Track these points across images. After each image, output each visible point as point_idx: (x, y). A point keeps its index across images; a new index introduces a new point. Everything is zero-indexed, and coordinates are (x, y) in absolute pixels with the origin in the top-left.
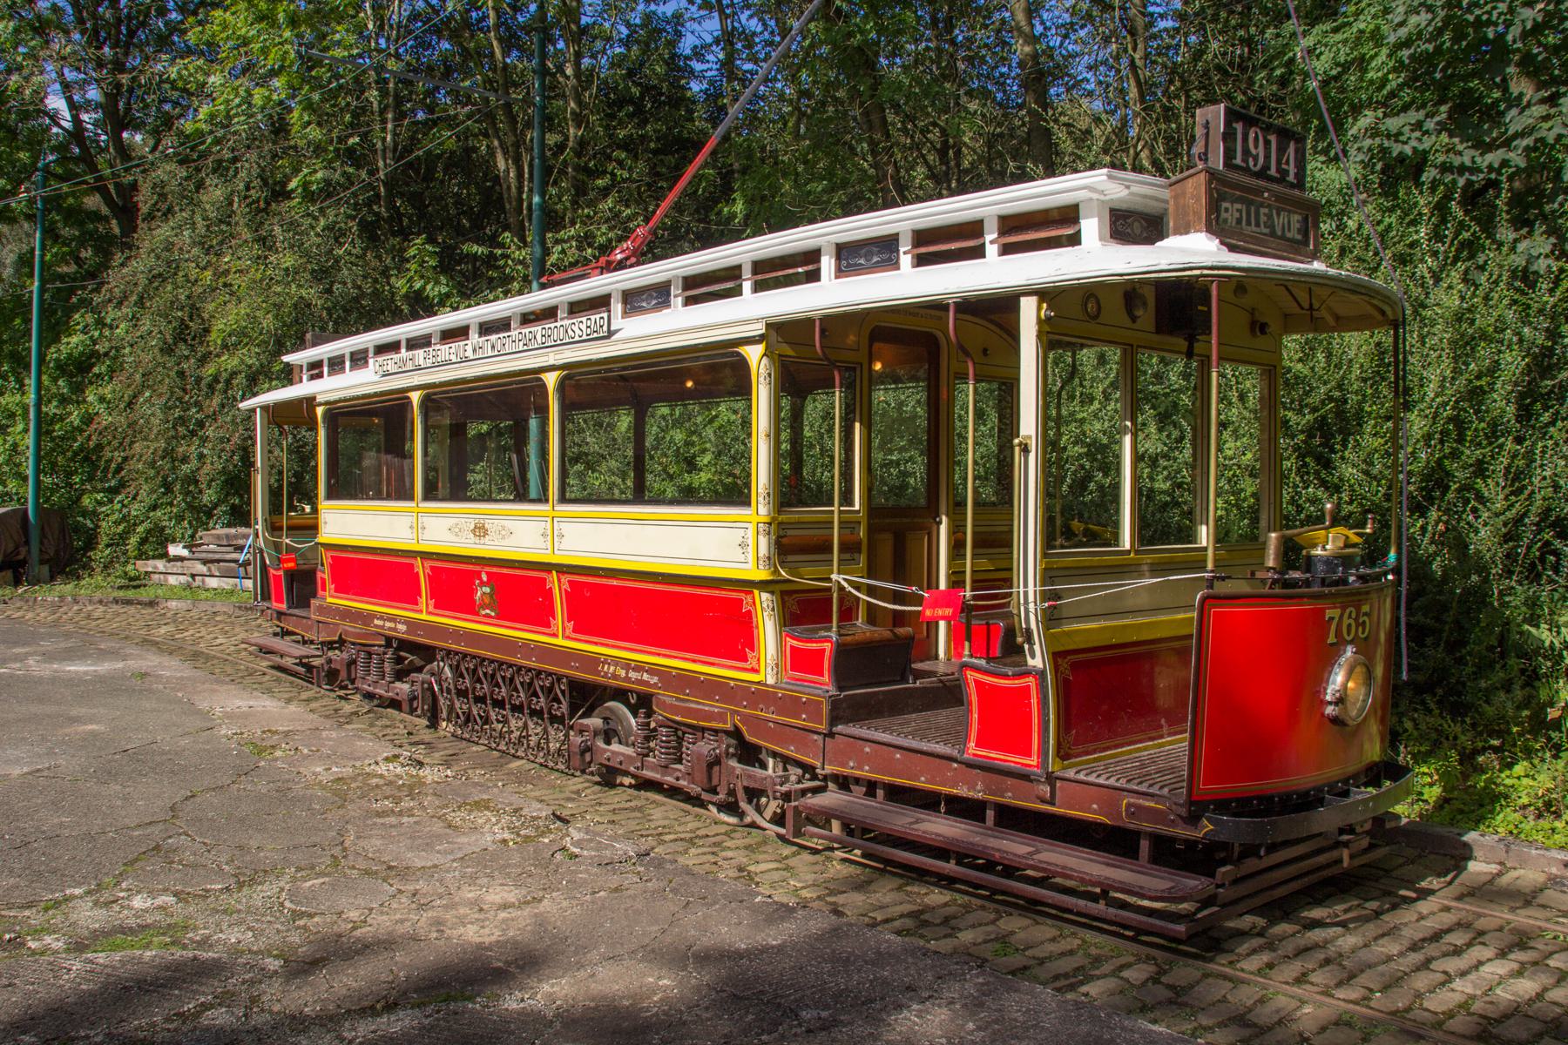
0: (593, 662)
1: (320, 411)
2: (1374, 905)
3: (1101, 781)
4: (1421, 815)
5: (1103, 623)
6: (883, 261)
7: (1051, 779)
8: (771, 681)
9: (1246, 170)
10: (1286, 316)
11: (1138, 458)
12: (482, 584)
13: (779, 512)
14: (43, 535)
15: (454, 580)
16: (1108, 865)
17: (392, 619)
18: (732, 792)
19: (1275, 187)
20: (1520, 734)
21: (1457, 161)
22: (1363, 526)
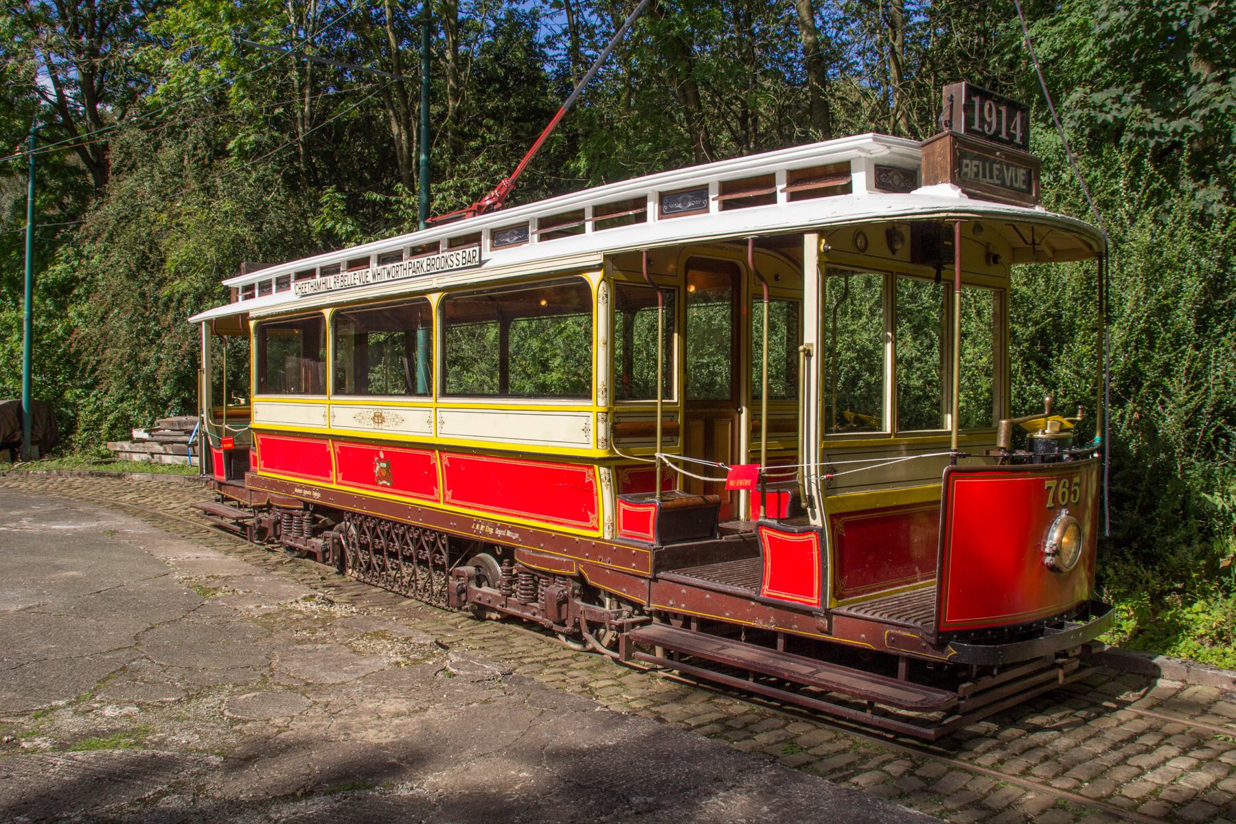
0: (467, 522)
1: (252, 324)
2: (1083, 713)
3: (868, 616)
4: (1120, 643)
5: (869, 492)
6: (696, 206)
7: (828, 614)
8: (607, 537)
9: (982, 134)
10: (1014, 249)
11: (897, 361)
12: (380, 460)
13: (614, 404)
14: (34, 422)
15: (358, 457)
16: (873, 682)
17: (309, 488)
18: (577, 625)
19: (1005, 147)
20: (1198, 579)
21: (1148, 127)
22: (1075, 414)
